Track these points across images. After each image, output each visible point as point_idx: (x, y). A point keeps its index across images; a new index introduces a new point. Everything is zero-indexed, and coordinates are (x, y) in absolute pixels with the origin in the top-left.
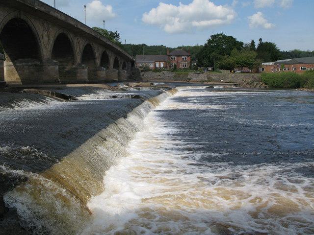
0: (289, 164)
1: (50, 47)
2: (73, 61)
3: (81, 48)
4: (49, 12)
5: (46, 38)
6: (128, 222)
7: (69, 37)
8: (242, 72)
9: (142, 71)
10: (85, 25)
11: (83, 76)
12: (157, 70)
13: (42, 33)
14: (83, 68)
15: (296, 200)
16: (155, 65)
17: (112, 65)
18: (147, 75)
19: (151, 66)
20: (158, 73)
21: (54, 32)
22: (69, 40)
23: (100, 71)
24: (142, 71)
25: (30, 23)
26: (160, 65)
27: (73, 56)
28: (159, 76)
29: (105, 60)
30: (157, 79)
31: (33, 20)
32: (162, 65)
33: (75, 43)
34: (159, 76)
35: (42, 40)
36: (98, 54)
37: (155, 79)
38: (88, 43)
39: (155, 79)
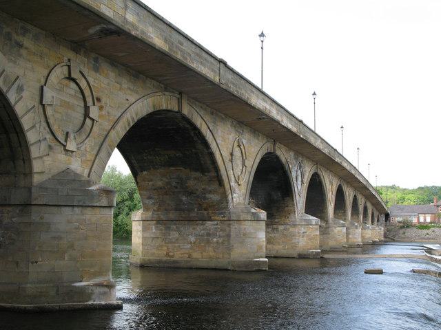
1: (246, 178)
5: (331, 193)
9: (402, 227)
10: (314, 132)
11: (355, 238)
12: (423, 226)
14: (357, 228)
17: (349, 213)
18: (410, 232)
19: (415, 220)
20: (425, 231)
21: (255, 149)
24: (402, 227)
26: (425, 219)
28: (428, 234)
29: (315, 204)
30: (424, 239)
31: (345, 186)
32: (428, 220)
34: (428, 234)
37: (422, 239)
39: (422, 239)
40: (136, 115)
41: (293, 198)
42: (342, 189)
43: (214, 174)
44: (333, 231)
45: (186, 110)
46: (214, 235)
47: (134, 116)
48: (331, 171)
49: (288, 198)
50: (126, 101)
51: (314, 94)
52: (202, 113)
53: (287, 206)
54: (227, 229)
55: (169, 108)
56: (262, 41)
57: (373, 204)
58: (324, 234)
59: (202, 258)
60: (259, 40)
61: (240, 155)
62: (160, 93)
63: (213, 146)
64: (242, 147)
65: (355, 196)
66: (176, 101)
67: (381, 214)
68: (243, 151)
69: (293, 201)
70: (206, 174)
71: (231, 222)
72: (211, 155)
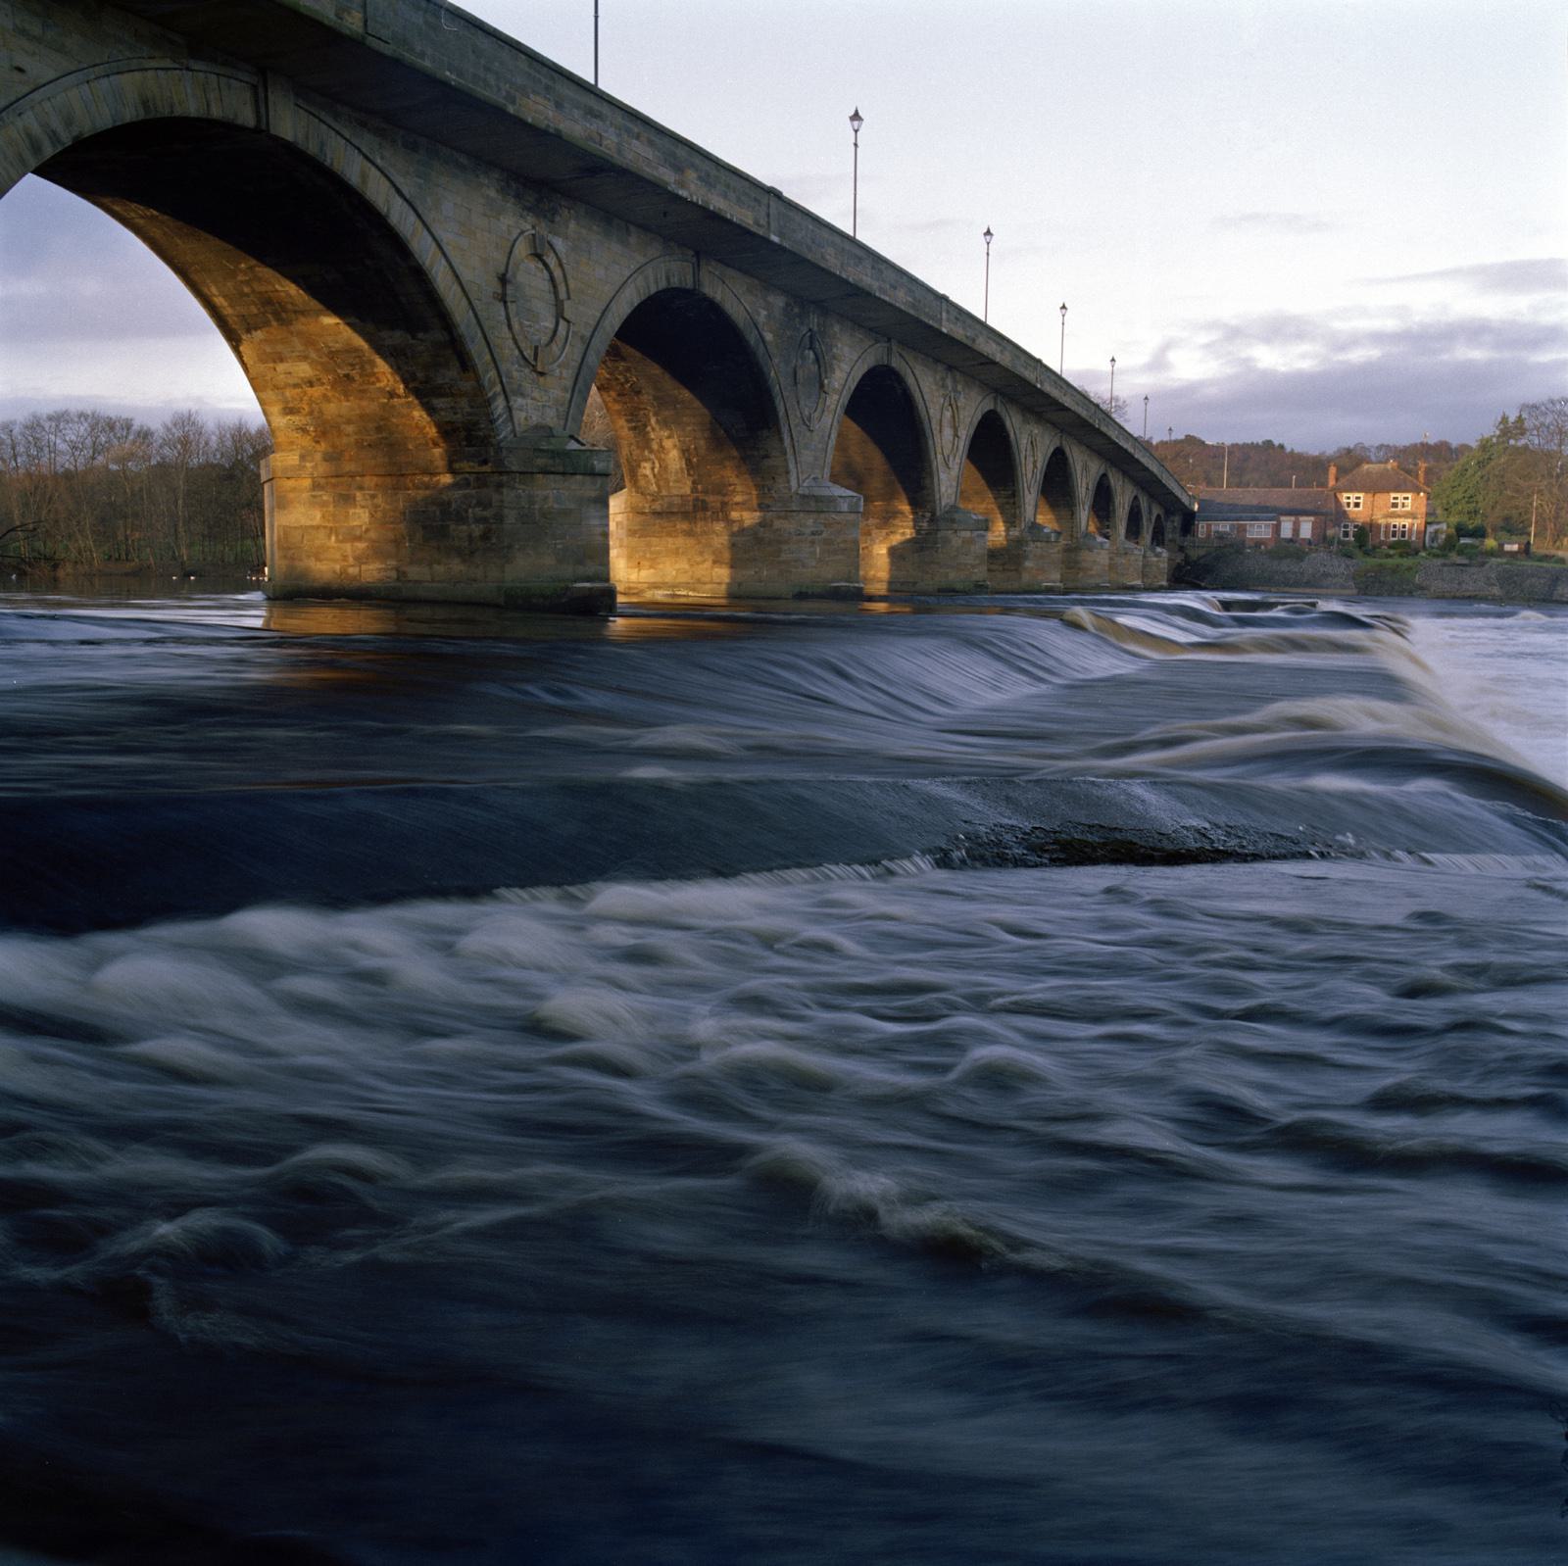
0: (1008, 813)
2: (1014, 516)
3: (1039, 465)
4: (974, 341)
5: (948, 432)
6: (45, 417)
7: (1008, 424)
8: (569, 298)
13: (938, 417)
15: (1190, 1109)
16: (1277, 529)
17: (1122, 529)
21: (972, 407)
22: (1008, 436)
23: (1090, 550)
25: (910, 381)
26: (1296, 530)
27: (1014, 495)
33: (1023, 447)
35: (937, 439)
36: (1084, 486)
38: (1058, 444)
40: (69, 122)
41: (779, 432)
42: (1109, 488)
43: (439, 335)
44: (947, 541)
45: (289, 122)
46: (461, 519)
47: (57, 124)
48: (950, 368)
49: (765, 433)
50: (16, 75)
51: (1064, 307)
52: (367, 141)
53: (767, 456)
54: (495, 497)
55: (216, 112)
56: (856, 131)
57: (1152, 496)
58: (922, 549)
59: (433, 581)
60: (1059, 313)
61: (546, 286)
62: (168, 63)
63: (422, 246)
64: (552, 261)
65: (1136, 498)
66: (248, 95)
67: (1168, 513)
68: (557, 273)
69: (781, 440)
70: (420, 335)
71: (504, 478)
72: (420, 274)
